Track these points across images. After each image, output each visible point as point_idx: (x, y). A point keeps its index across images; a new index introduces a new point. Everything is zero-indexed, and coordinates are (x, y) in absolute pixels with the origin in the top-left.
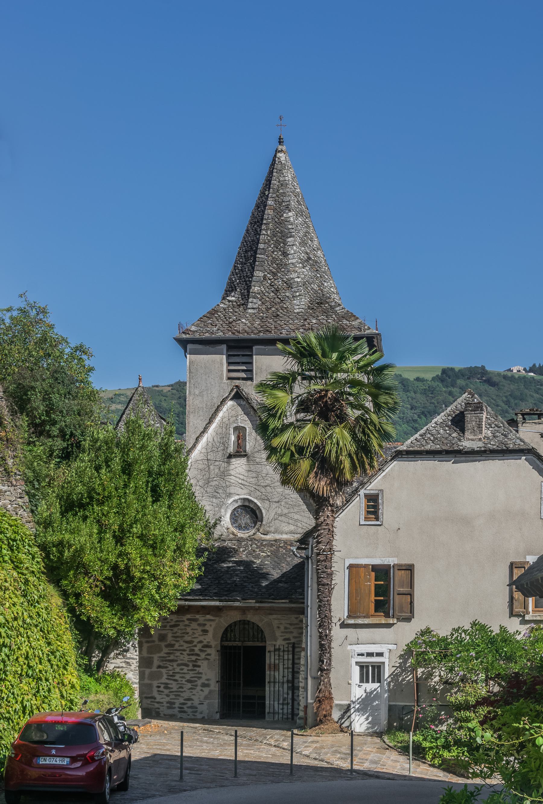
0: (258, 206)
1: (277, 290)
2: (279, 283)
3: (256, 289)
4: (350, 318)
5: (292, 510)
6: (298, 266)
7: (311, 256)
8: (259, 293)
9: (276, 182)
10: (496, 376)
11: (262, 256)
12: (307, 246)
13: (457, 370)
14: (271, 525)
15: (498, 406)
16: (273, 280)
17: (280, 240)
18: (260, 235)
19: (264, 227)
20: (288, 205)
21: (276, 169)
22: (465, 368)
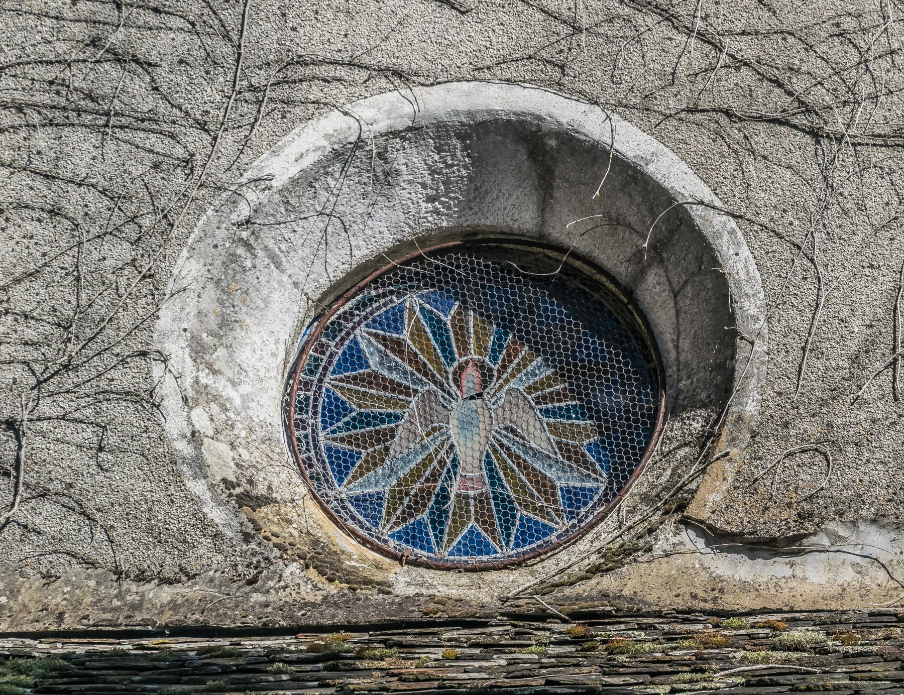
14: (849, 419)
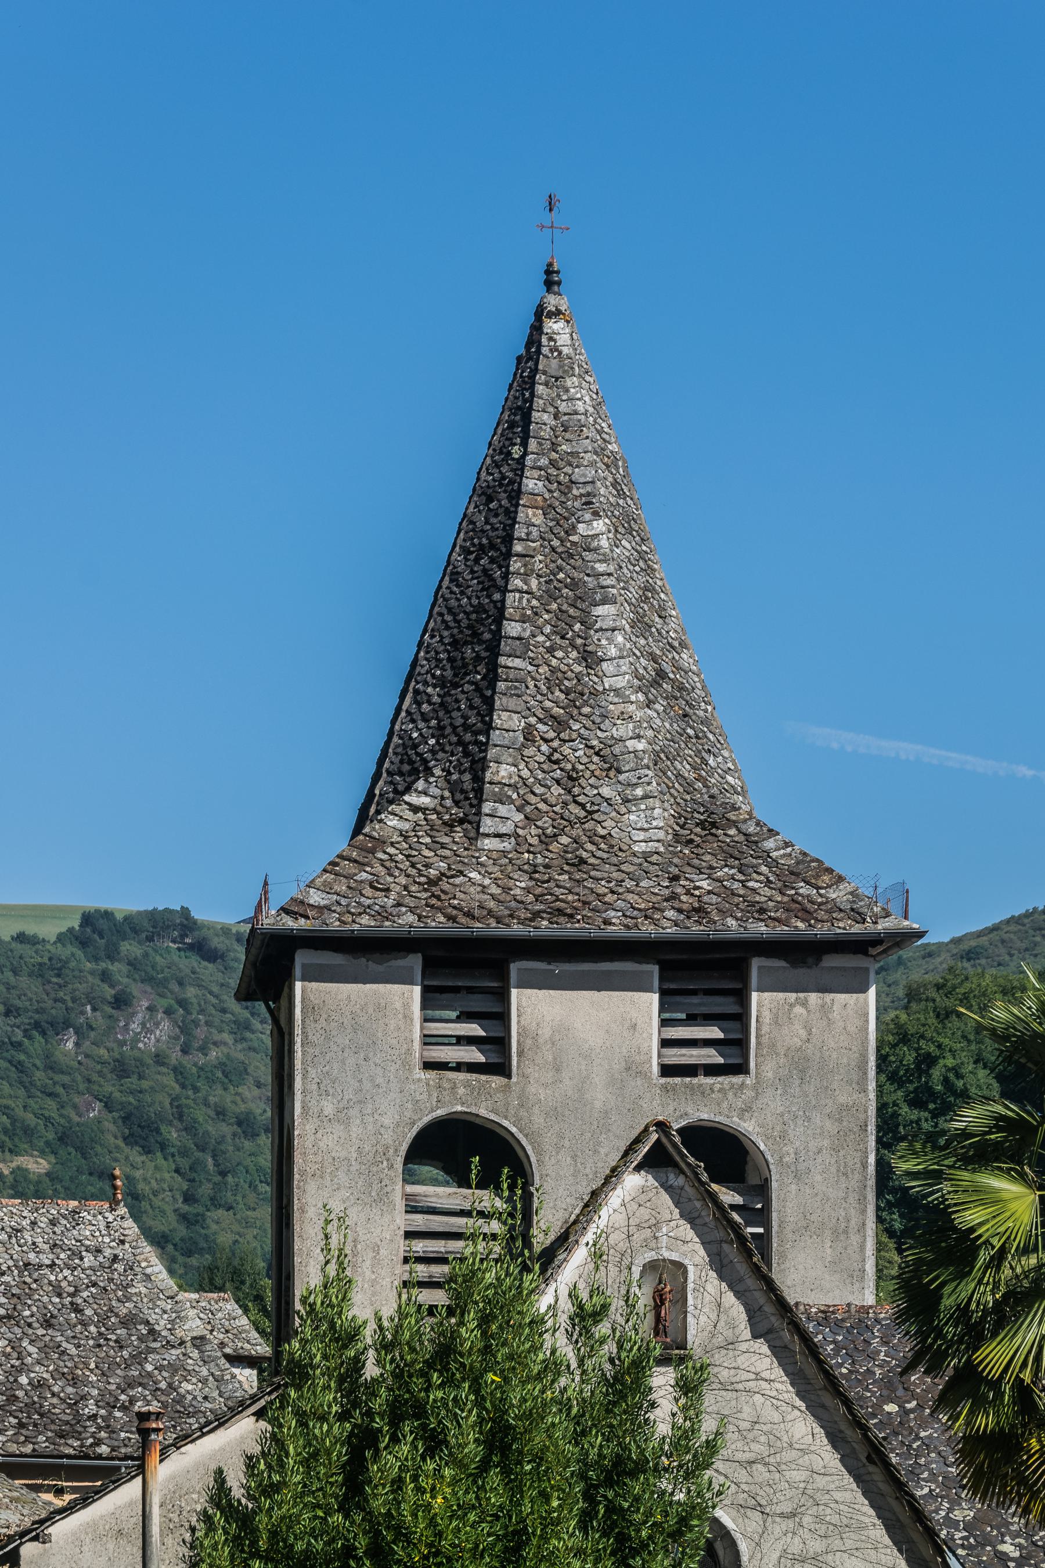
0: (484, 494)
1: (570, 778)
2: (576, 753)
3: (501, 771)
4: (817, 877)
5: (837, 1544)
6: (633, 698)
7: (668, 668)
8: (514, 787)
9: (545, 416)
10: (217, 935)
11: (517, 663)
12: (651, 634)
13: (119, 917)
15: (224, 1011)
16: (556, 744)
17: (571, 611)
18: (504, 591)
19: (515, 565)
20: (589, 494)
21: (545, 373)
22: (139, 913)
